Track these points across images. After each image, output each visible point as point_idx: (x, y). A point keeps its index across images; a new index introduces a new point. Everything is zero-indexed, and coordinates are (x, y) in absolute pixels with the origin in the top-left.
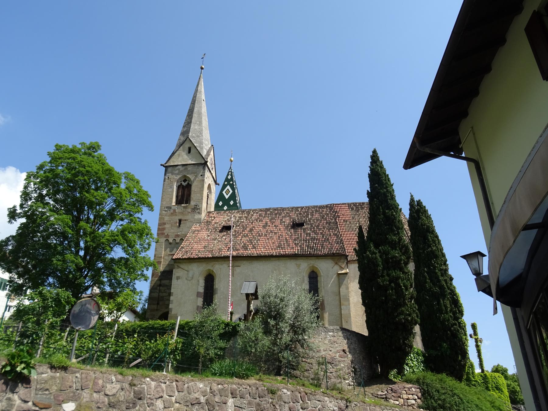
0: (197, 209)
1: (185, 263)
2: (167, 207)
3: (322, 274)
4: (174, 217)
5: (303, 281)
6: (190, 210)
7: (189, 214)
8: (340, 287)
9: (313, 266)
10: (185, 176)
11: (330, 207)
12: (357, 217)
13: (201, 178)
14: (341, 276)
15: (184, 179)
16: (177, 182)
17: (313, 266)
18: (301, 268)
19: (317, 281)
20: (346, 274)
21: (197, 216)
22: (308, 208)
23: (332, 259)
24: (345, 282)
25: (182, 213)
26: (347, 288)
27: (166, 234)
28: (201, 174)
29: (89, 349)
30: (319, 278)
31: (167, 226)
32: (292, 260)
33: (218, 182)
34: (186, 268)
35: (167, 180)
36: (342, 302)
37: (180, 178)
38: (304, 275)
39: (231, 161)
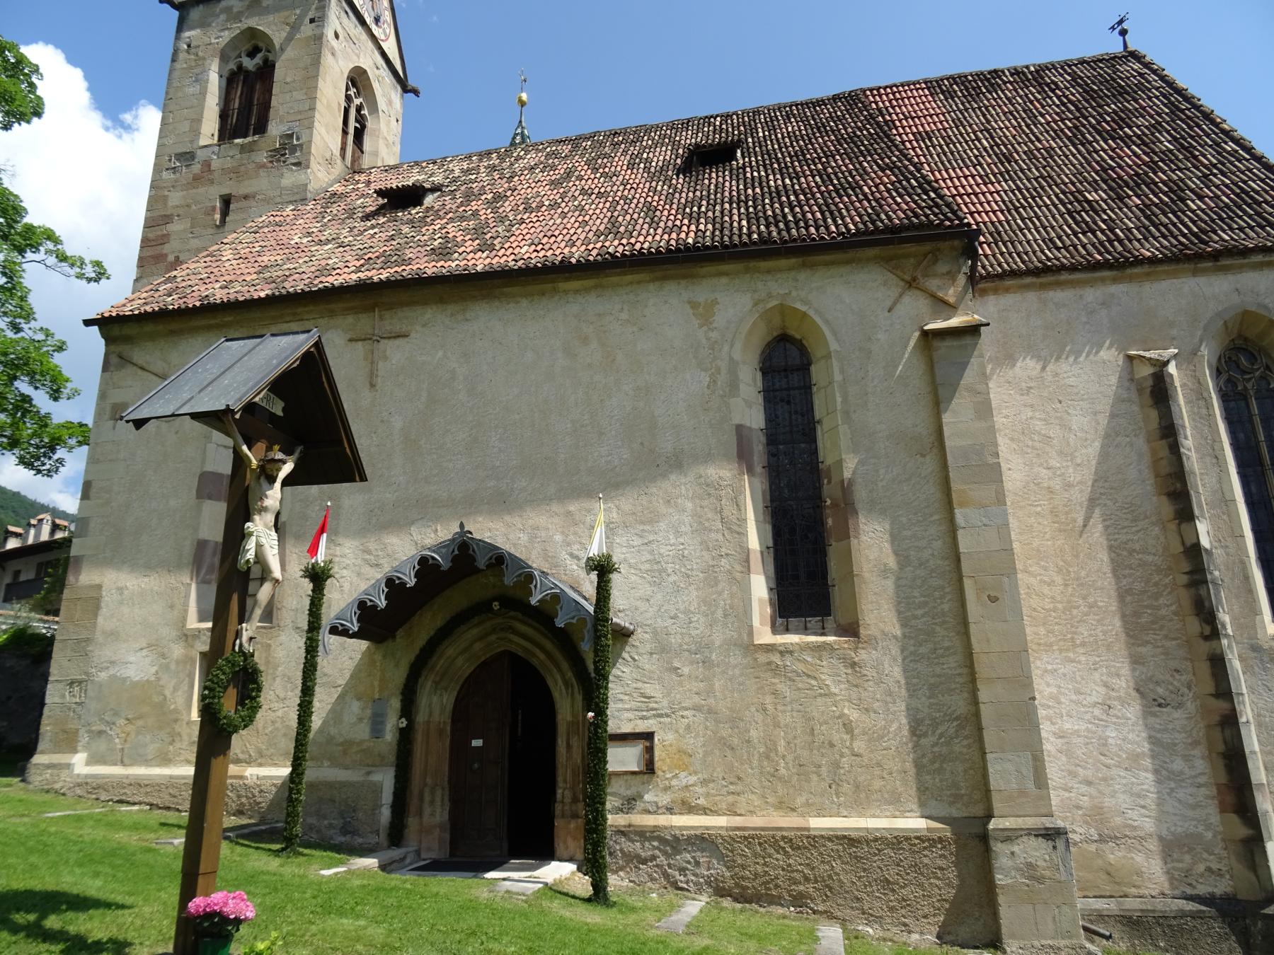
0: (294, 149)
1: (152, 337)
2: (180, 156)
3: (834, 346)
4: (202, 190)
5: (734, 387)
6: (262, 157)
7: (262, 173)
8: (938, 404)
9: (783, 310)
10: (252, 33)
11: (852, 100)
12: (975, 119)
13: (307, 30)
14: (937, 343)
15: (248, 46)
16: (224, 58)
17: (783, 310)
18: (720, 319)
19: (807, 388)
20: (973, 331)
21: (290, 178)
22: (757, 112)
23: (886, 261)
24: (969, 377)
25: (236, 173)
26: (984, 410)
27: (171, 258)
28: (311, 15)
29: (877, 471)
30: (816, 371)
31: (176, 227)
32: (671, 286)
33: (412, 82)
34: (158, 366)
35: (182, 56)
36: (955, 486)
37: (233, 43)
38: (737, 355)
39: (522, 104)
